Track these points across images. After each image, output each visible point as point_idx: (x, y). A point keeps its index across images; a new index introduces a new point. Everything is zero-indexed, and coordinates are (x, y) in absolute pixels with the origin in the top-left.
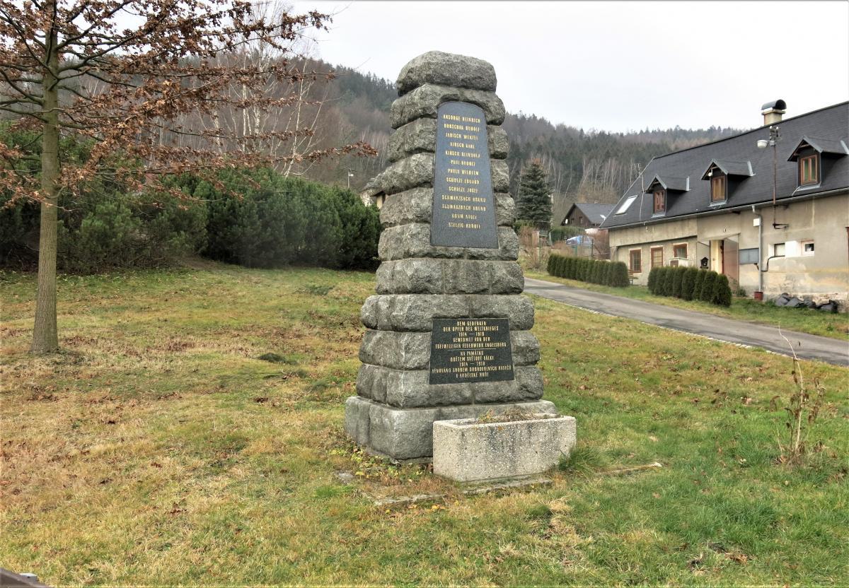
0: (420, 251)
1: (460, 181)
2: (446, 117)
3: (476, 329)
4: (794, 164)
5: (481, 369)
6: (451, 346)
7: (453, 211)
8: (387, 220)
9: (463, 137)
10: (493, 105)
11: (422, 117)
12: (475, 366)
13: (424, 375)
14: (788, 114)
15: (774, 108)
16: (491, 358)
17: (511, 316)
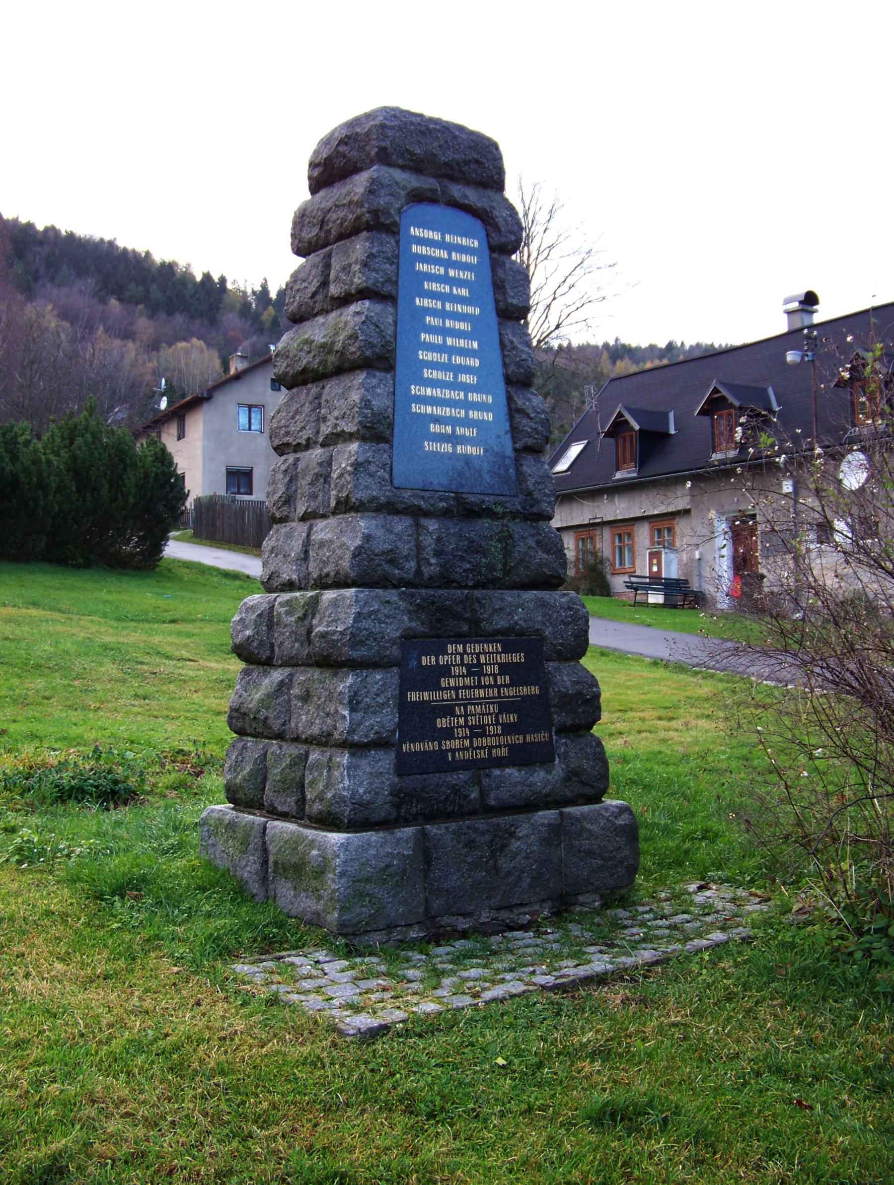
0: (373, 499)
1: (444, 358)
2: (415, 231)
3: (482, 660)
4: (706, 419)
5: (494, 741)
6: (436, 695)
7: (437, 420)
8: (290, 439)
9: (446, 272)
10: (500, 214)
11: (369, 228)
12: (483, 735)
13: (385, 760)
14: (822, 314)
15: (801, 302)
16: (513, 718)
17: (548, 632)
